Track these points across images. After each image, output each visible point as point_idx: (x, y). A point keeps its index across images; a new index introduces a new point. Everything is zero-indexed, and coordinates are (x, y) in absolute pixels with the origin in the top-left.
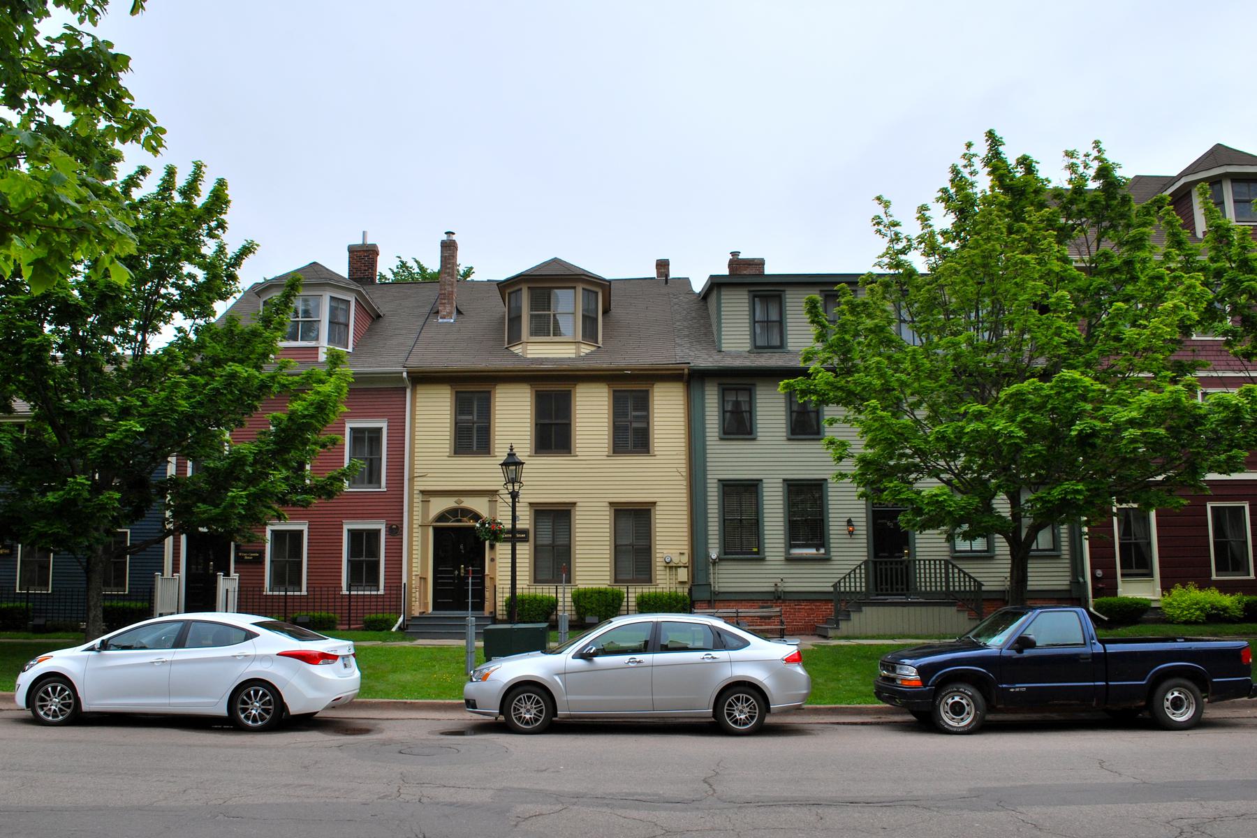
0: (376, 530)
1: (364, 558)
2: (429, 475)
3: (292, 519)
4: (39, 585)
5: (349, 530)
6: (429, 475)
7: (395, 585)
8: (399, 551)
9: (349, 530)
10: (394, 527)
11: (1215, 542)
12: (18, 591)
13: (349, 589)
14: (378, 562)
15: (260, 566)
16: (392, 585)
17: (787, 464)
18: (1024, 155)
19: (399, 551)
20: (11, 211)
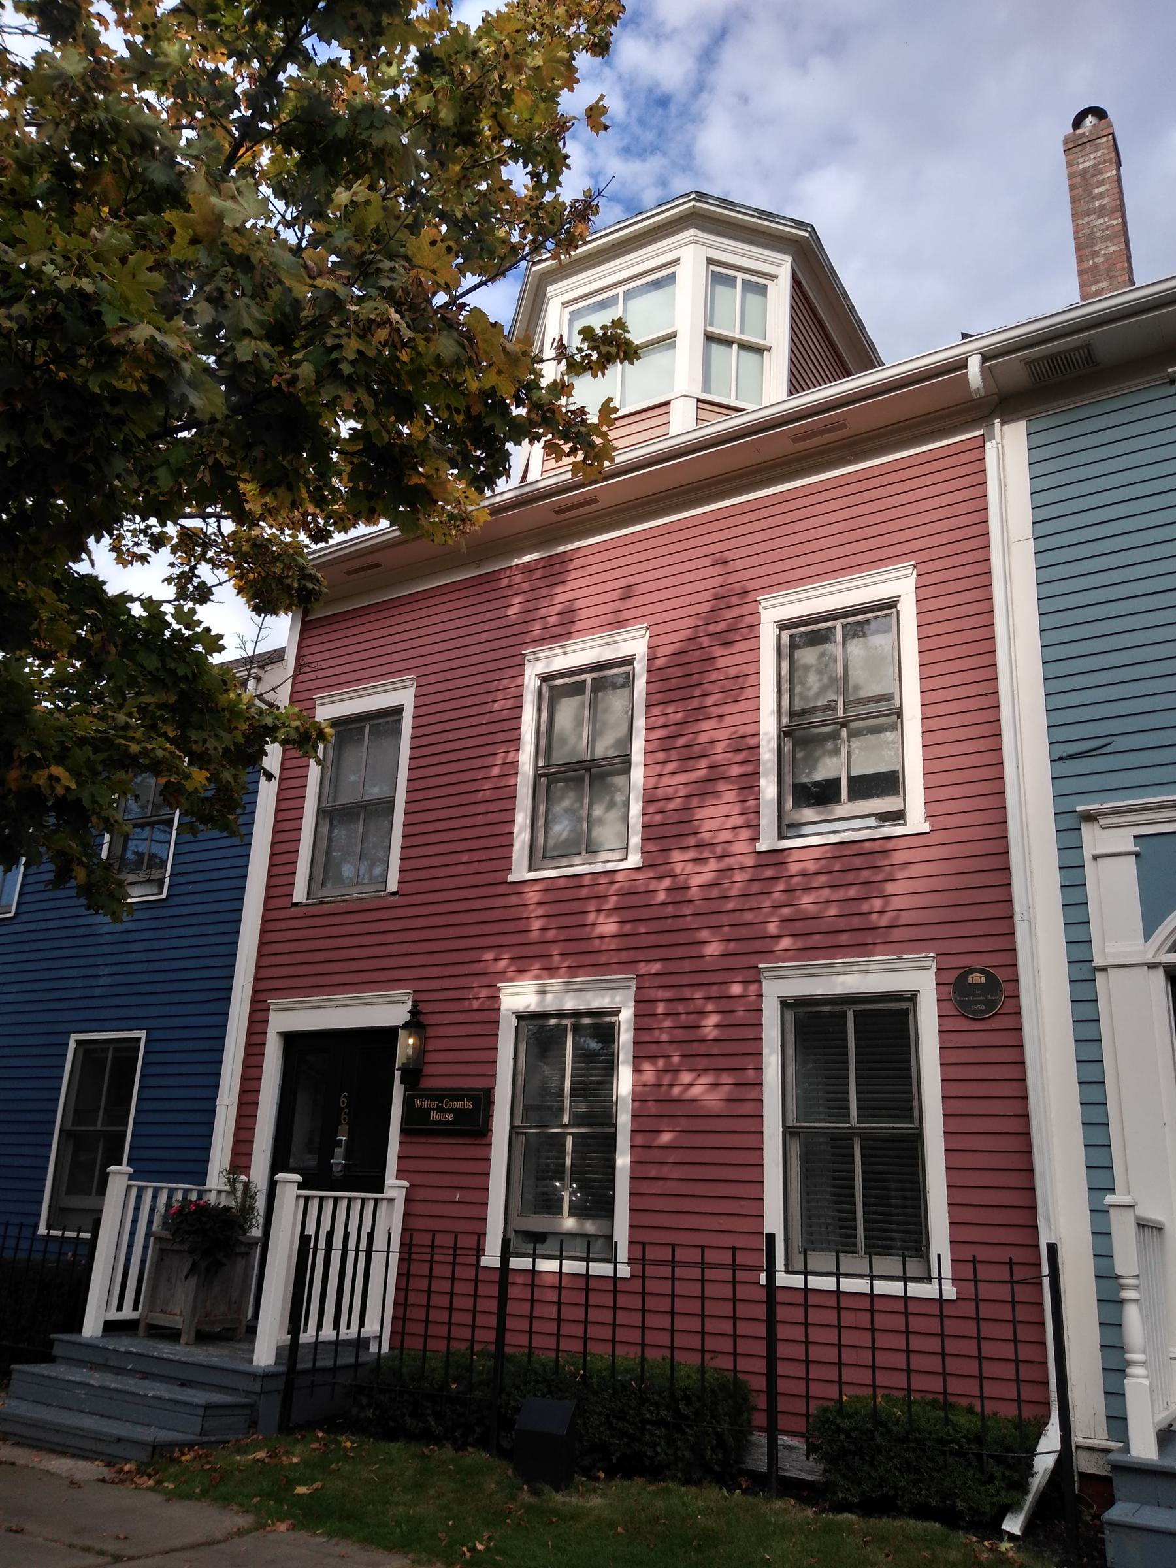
0: (897, 997)
1: (99, 1127)
2: (1119, 744)
3: (803, 952)
4: (878, 1246)
5: (786, 1004)
6: (1119, 744)
7: (1004, 1254)
8: (1008, 1090)
9: (786, 1004)
10: (978, 978)
11: (126, 1125)
12: (42, 1231)
13: (49, 1227)
14: (915, 1141)
15: (477, 1152)
16: (983, 1254)
17: (201, 919)
18: (626, 160)
19: (1008, 1090)
20: (156, 55)
